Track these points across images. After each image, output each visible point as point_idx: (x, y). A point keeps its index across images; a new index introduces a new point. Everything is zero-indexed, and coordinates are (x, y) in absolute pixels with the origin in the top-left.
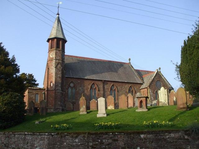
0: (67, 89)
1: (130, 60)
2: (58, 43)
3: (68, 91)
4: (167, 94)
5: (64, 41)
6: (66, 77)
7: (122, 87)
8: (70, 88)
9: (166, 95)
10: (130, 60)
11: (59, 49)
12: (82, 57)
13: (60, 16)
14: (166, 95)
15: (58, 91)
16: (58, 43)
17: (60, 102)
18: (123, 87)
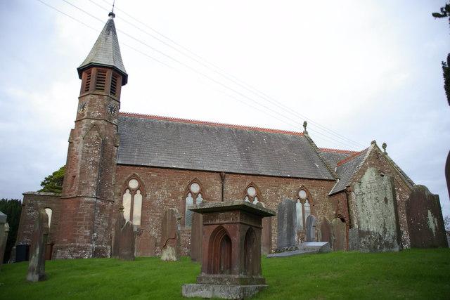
0: (121, 195)
1: (305, 124)
2: (102, 78)
3: (121, 201)
4: (390, 197)
5: (121, 77)
6: (118, 164)
7: (277, 191)
8: (128, 191)
9: (386, 200)
10: (305, 124)
11: (100, 93)
12: (180, 120)
13: (115, 19)
14: (386, 200)
15: (86, 199)
16: (102, 78)
17: (90, 228)
18: (281, 190)
